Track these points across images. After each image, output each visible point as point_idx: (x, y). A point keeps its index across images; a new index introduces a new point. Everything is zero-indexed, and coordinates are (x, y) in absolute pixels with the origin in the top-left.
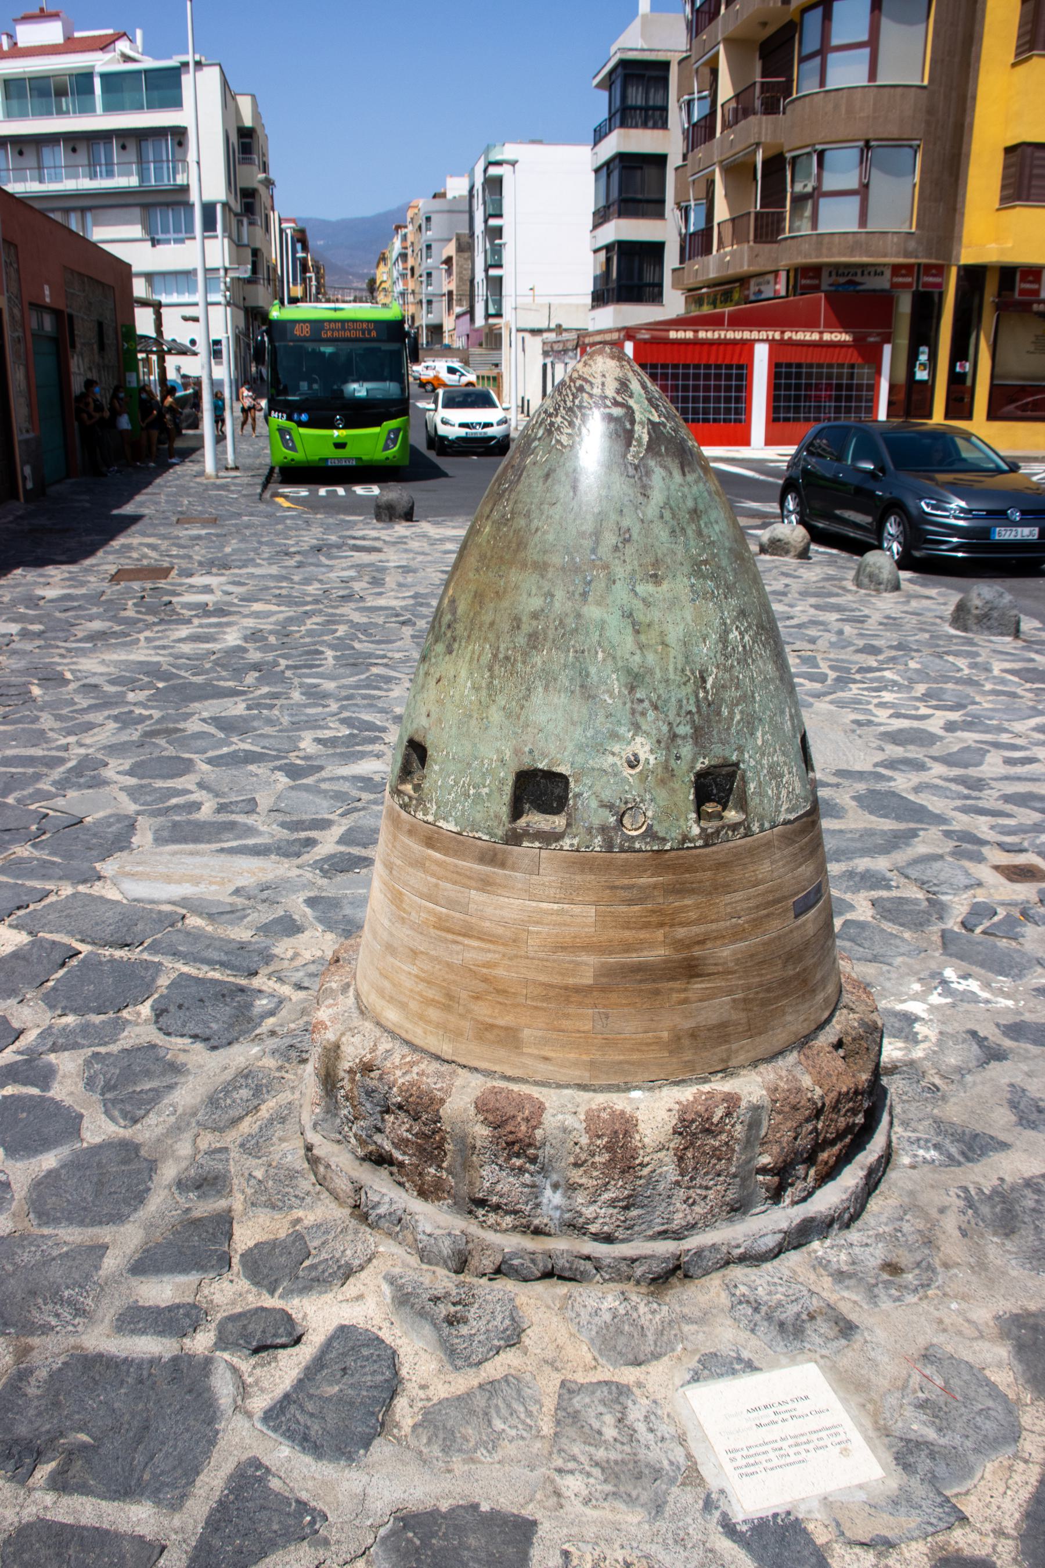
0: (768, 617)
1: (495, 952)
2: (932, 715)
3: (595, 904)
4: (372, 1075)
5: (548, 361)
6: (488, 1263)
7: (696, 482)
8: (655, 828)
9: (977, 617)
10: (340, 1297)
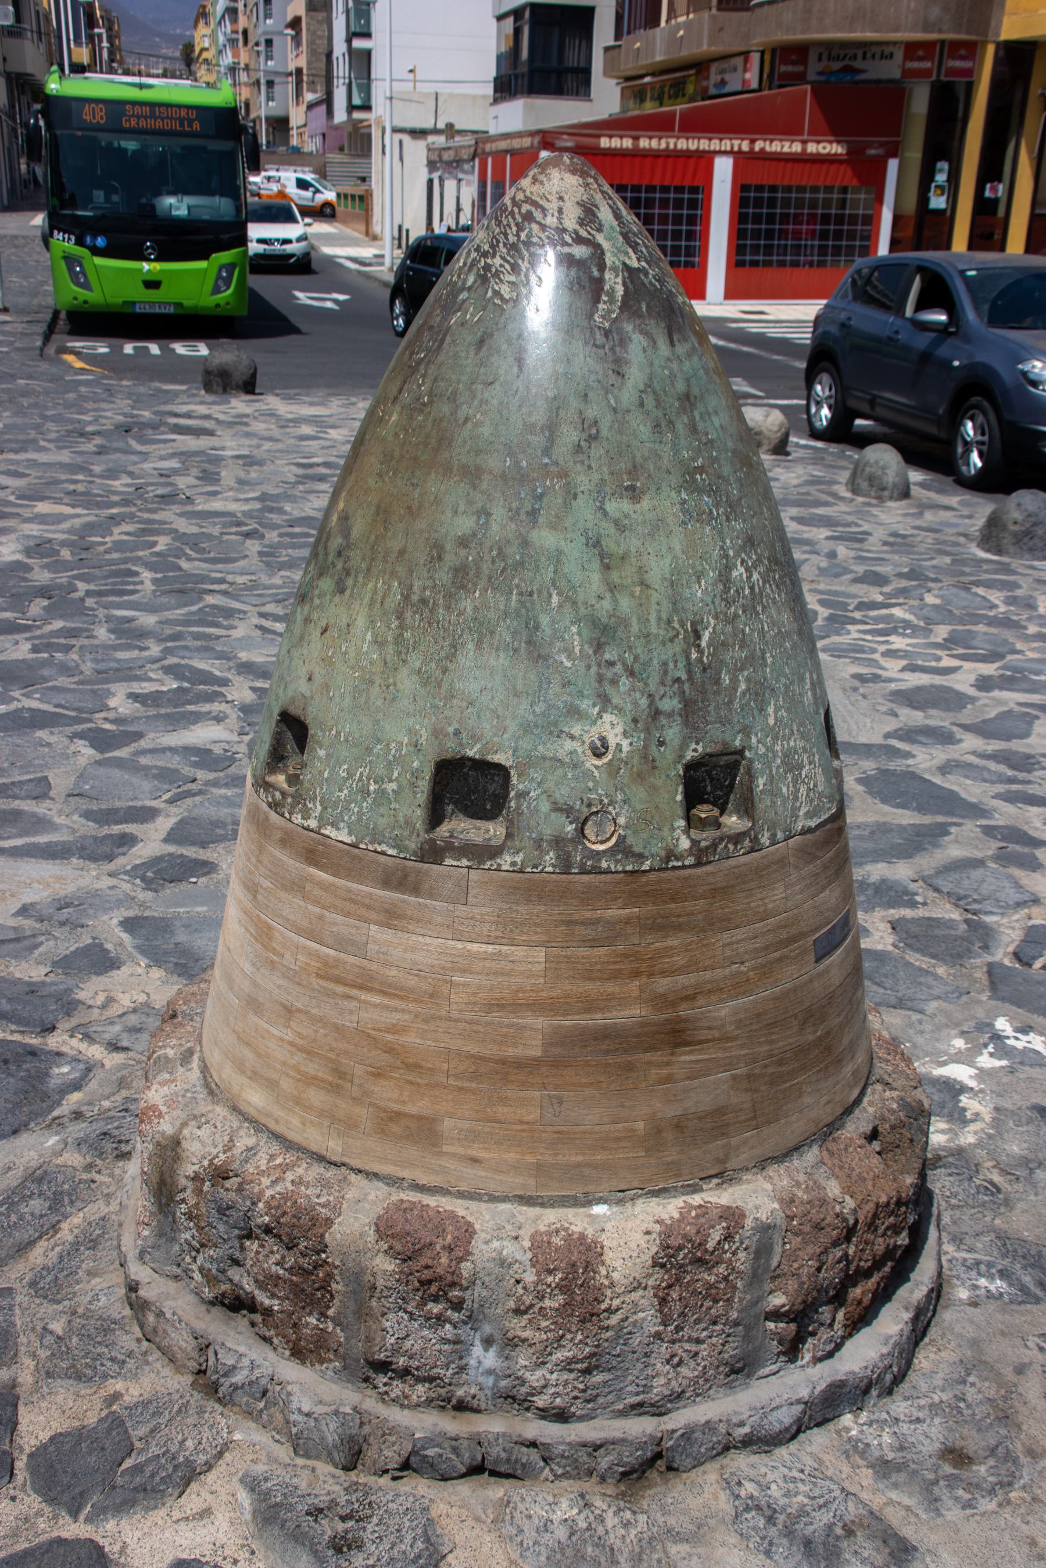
0: (783, 546)
1: (403, 1011)
2: (960, 667)
3: (545, 945)
4: (228, 1184)
5: (435, 176)
6: (392, 1455)
7: (689, 355)
8: (630, 841)
9: (1015, 534)
10: (177, 1514)
